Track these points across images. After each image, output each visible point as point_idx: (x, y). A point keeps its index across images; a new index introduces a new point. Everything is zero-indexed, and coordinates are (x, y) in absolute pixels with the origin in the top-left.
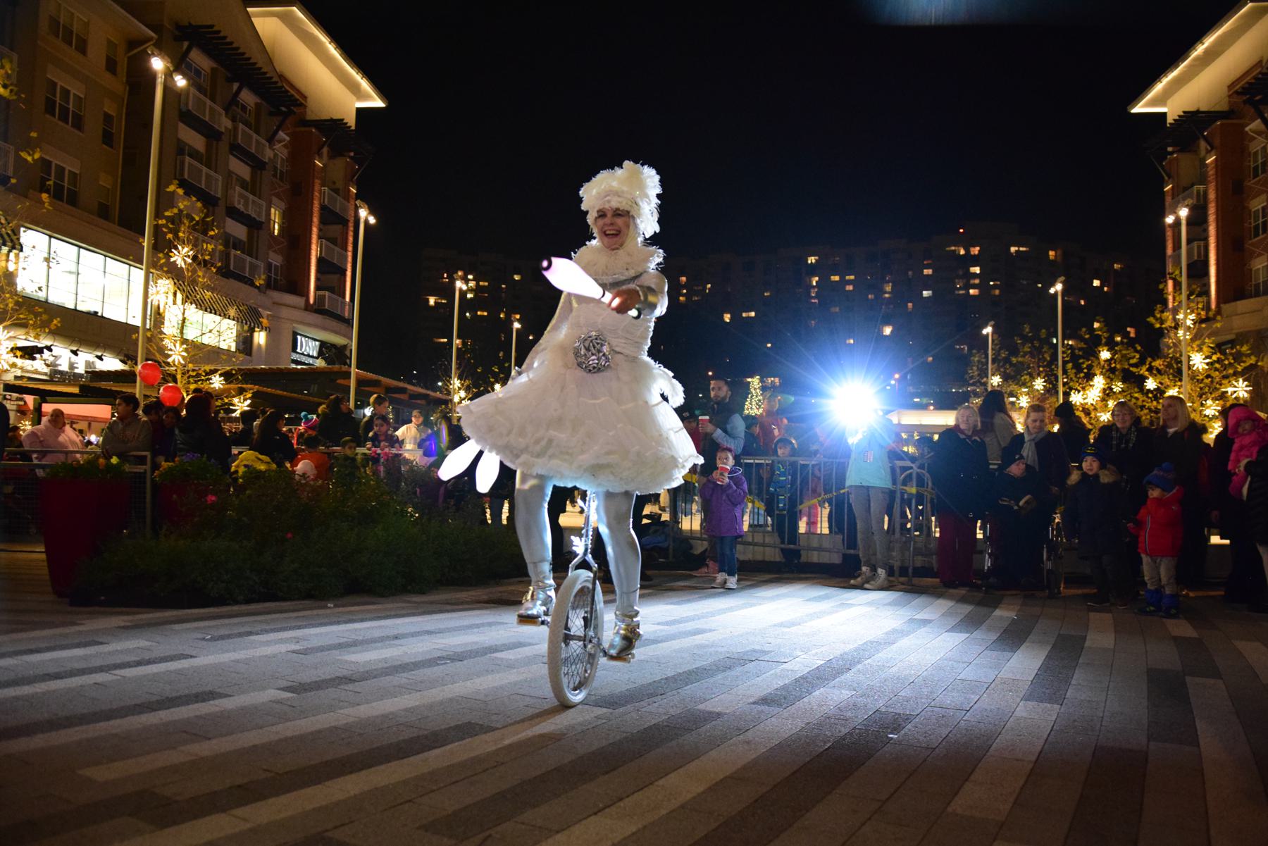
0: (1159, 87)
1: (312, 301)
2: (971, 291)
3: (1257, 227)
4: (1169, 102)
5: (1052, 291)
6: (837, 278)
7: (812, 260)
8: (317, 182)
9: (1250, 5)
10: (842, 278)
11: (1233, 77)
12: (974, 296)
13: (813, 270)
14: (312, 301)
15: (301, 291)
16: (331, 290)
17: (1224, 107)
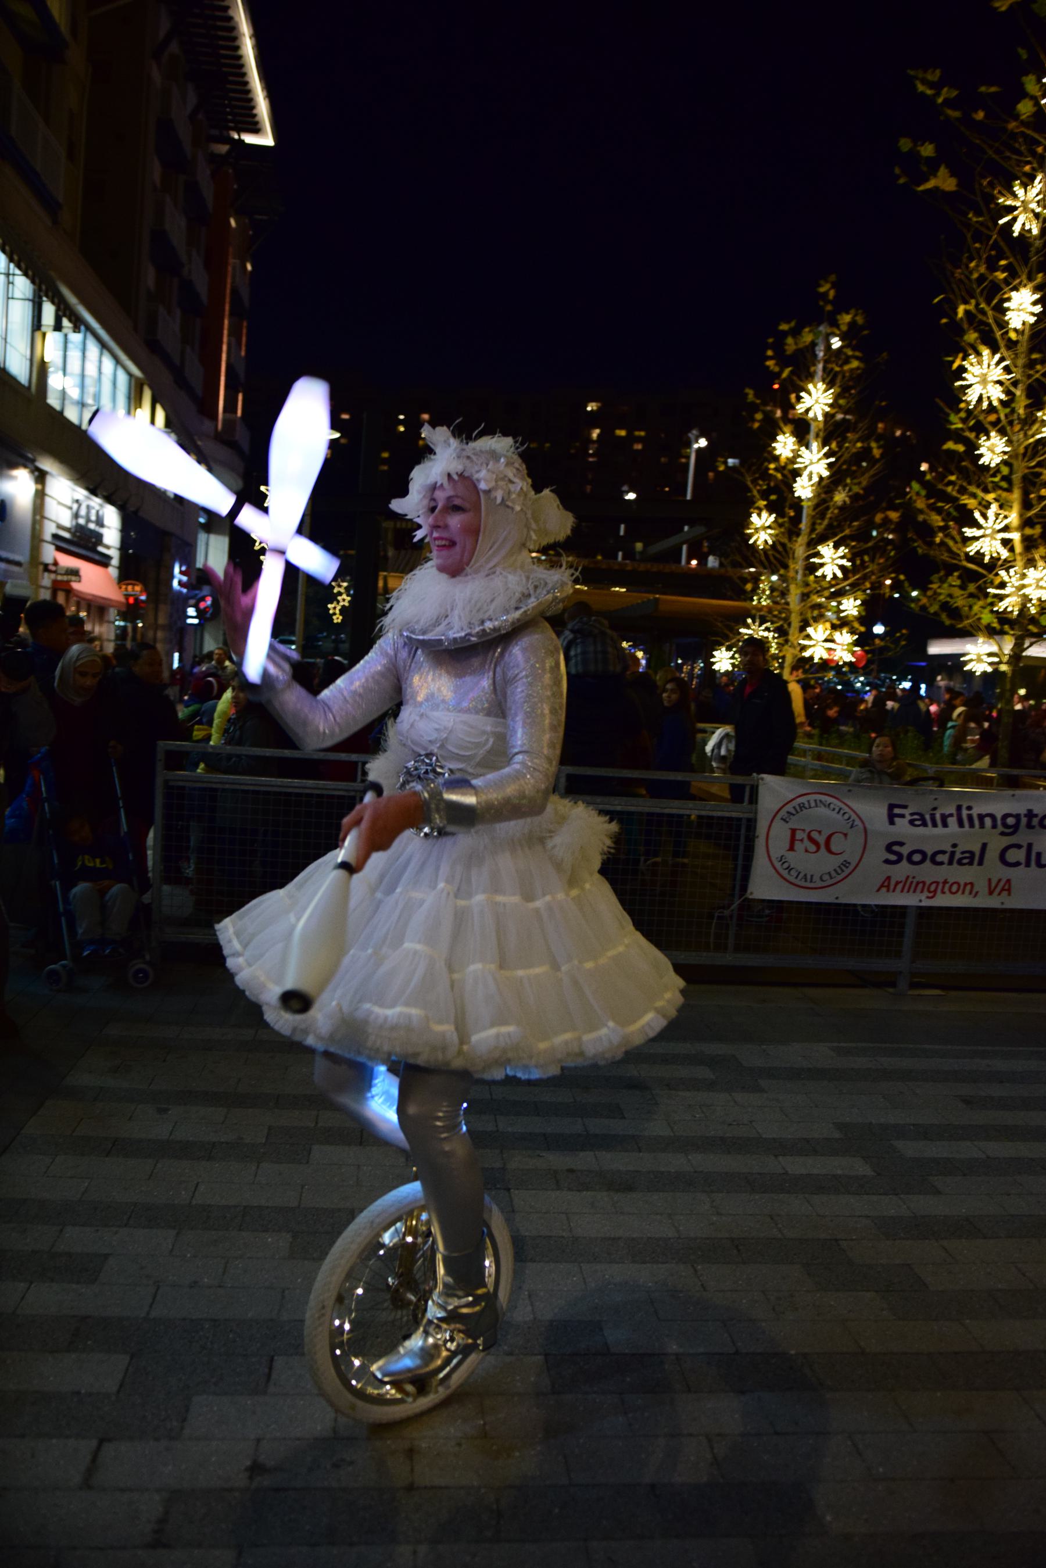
6: (622, 433)
10: (630, 433)
13: (593, 420)
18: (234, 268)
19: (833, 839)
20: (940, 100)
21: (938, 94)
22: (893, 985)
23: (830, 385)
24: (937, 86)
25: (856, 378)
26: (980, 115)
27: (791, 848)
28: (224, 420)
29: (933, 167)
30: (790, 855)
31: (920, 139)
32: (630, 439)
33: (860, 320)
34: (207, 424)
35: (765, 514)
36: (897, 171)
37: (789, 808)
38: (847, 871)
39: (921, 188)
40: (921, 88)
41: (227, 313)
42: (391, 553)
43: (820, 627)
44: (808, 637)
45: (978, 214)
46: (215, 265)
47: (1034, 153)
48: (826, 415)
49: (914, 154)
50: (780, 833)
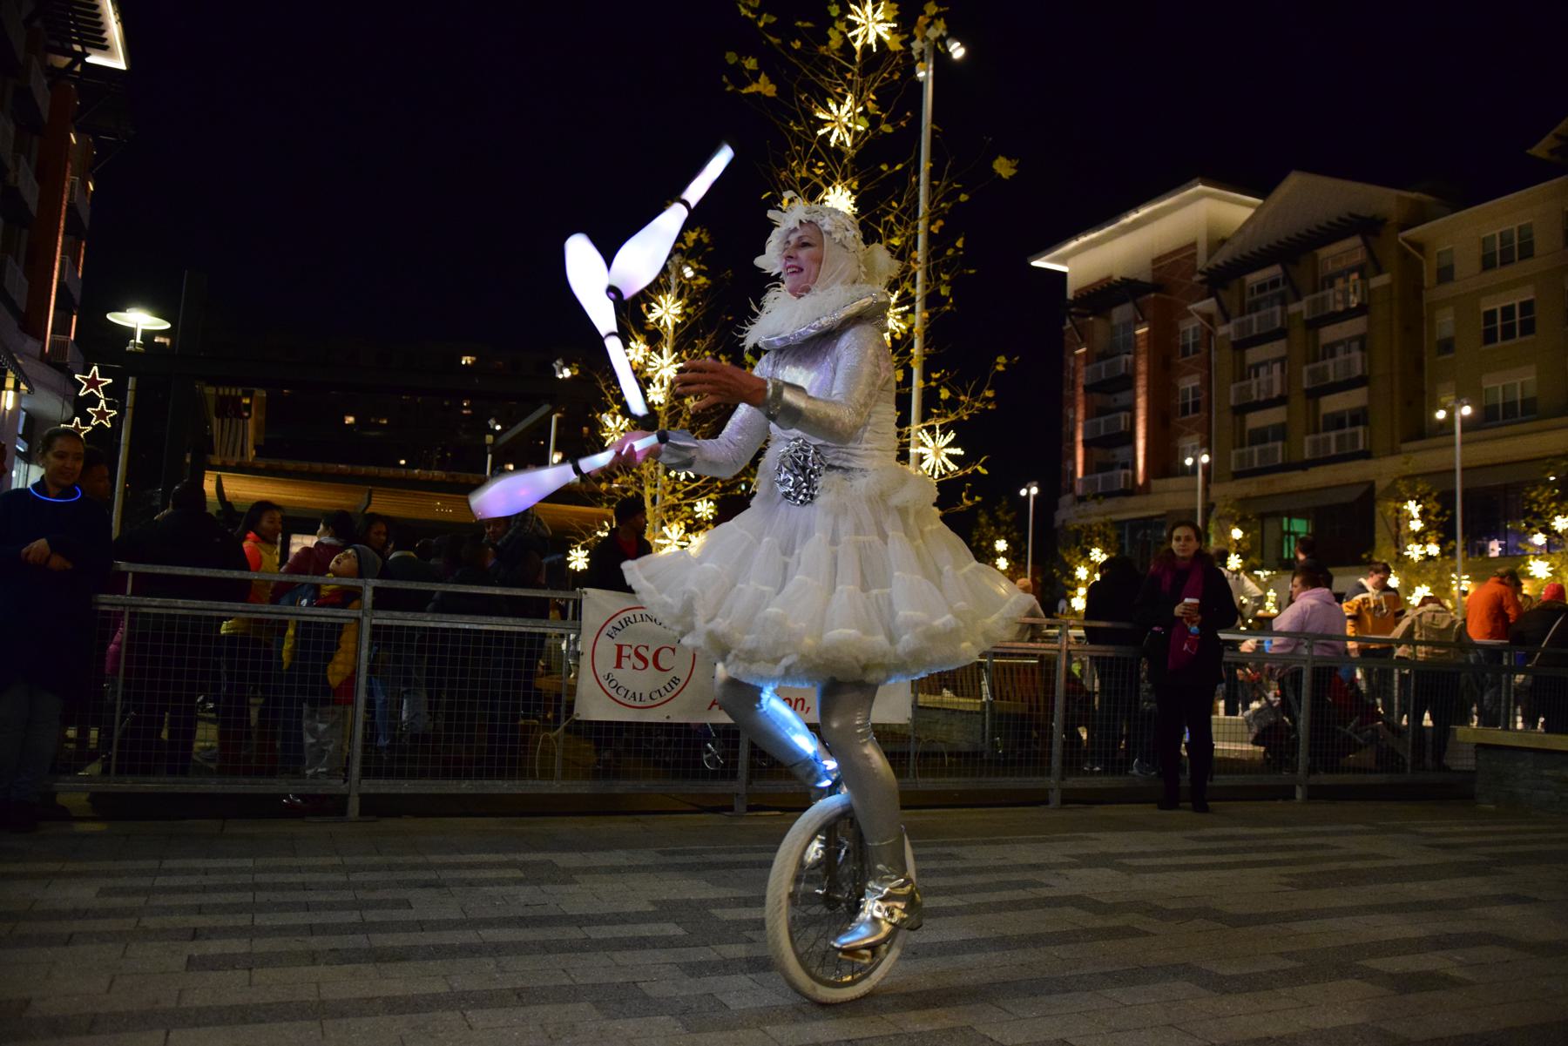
0: (1073, 244)
3: (1185, 406)
4: (1071, 261)
5: (1023, 492)
9: (1200, 187)
11: (1157, 253)
17: (1146, 277)
18: (72, 185)
19: (661, 655)
20: (761, 24)
21: (759, 18)
22: (731, 809)
23: (679, 296)
24: (758, 12)
25: (704, 292)
26: (797, 45)
27: (619, 665)
28: (53, 343)
29: (755, 76)
30: (617, 673)
31: (743, 53)
33: (706, 240)
34: (31, 344)
35: (619, 418)
36: (725, 79)
37: (614, 623)
38: (677, 688)
39: (745, 91)
40: (744, 11)
41: (62, 230)
42: (215, 421)
43: (675, 527)
44: (664, 537)
45: (798, 123)
46: (49, 177)
47: (844, 79)
48: (676, 326)
49: (739, 67)
50: (607, 648)
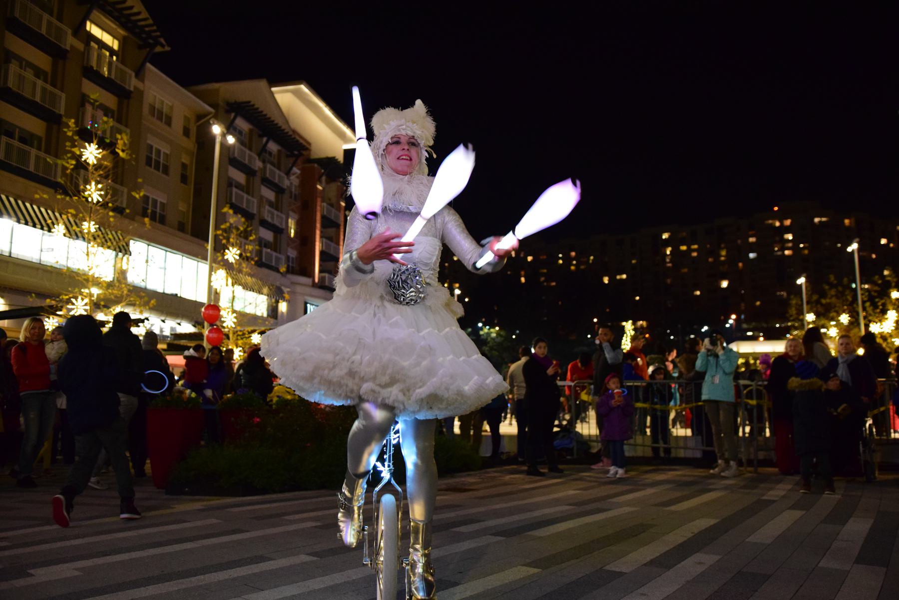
1: (317, 280)
2: (787, 252)
5: (849, 249)
6: (684, 248)
7: (665, 236)
8: (319, 200)
12: (788, 256)
13: (667, 243)
14: (317, 280)
15: (311, 275)
16: (330, 272)
32: (690, 250)
